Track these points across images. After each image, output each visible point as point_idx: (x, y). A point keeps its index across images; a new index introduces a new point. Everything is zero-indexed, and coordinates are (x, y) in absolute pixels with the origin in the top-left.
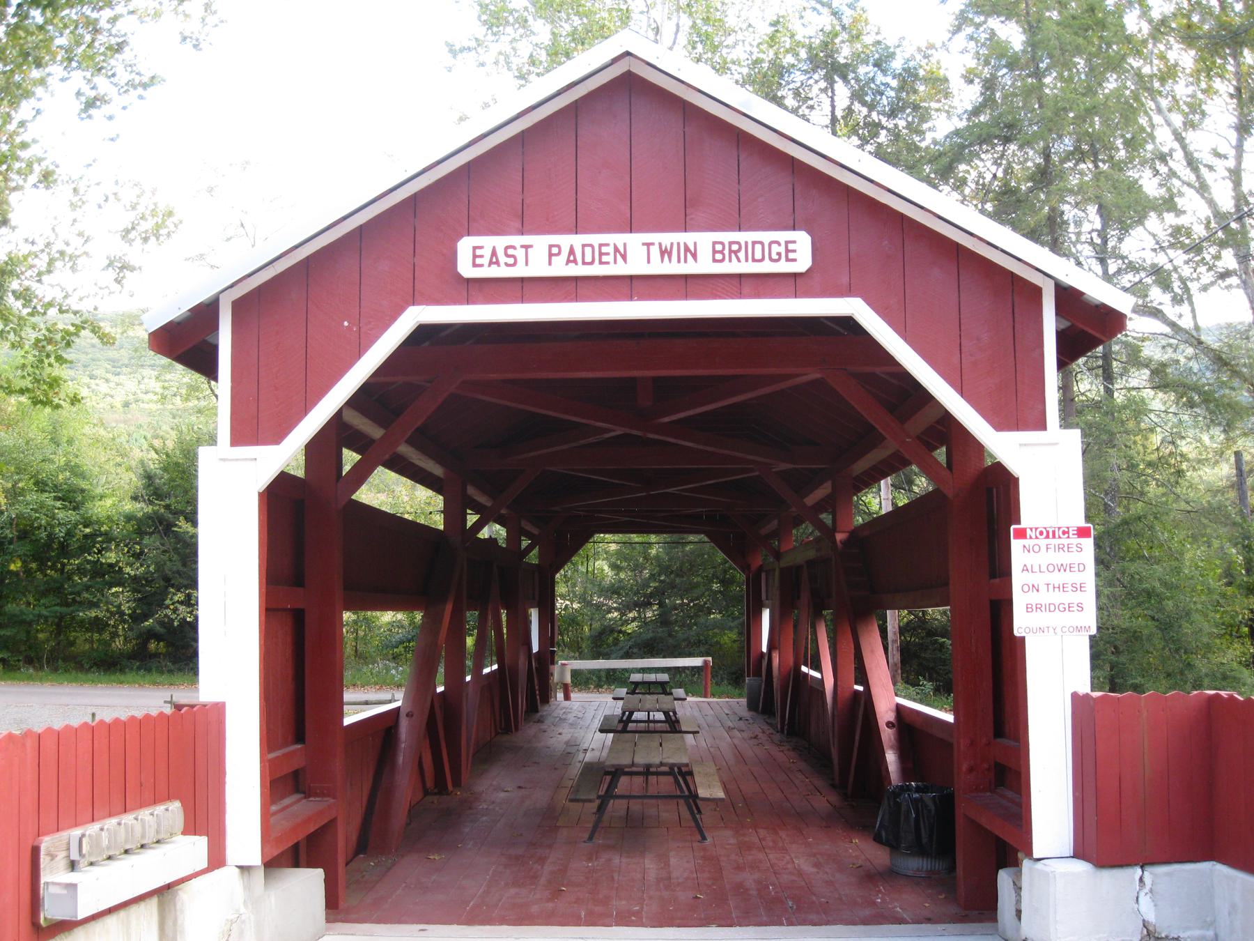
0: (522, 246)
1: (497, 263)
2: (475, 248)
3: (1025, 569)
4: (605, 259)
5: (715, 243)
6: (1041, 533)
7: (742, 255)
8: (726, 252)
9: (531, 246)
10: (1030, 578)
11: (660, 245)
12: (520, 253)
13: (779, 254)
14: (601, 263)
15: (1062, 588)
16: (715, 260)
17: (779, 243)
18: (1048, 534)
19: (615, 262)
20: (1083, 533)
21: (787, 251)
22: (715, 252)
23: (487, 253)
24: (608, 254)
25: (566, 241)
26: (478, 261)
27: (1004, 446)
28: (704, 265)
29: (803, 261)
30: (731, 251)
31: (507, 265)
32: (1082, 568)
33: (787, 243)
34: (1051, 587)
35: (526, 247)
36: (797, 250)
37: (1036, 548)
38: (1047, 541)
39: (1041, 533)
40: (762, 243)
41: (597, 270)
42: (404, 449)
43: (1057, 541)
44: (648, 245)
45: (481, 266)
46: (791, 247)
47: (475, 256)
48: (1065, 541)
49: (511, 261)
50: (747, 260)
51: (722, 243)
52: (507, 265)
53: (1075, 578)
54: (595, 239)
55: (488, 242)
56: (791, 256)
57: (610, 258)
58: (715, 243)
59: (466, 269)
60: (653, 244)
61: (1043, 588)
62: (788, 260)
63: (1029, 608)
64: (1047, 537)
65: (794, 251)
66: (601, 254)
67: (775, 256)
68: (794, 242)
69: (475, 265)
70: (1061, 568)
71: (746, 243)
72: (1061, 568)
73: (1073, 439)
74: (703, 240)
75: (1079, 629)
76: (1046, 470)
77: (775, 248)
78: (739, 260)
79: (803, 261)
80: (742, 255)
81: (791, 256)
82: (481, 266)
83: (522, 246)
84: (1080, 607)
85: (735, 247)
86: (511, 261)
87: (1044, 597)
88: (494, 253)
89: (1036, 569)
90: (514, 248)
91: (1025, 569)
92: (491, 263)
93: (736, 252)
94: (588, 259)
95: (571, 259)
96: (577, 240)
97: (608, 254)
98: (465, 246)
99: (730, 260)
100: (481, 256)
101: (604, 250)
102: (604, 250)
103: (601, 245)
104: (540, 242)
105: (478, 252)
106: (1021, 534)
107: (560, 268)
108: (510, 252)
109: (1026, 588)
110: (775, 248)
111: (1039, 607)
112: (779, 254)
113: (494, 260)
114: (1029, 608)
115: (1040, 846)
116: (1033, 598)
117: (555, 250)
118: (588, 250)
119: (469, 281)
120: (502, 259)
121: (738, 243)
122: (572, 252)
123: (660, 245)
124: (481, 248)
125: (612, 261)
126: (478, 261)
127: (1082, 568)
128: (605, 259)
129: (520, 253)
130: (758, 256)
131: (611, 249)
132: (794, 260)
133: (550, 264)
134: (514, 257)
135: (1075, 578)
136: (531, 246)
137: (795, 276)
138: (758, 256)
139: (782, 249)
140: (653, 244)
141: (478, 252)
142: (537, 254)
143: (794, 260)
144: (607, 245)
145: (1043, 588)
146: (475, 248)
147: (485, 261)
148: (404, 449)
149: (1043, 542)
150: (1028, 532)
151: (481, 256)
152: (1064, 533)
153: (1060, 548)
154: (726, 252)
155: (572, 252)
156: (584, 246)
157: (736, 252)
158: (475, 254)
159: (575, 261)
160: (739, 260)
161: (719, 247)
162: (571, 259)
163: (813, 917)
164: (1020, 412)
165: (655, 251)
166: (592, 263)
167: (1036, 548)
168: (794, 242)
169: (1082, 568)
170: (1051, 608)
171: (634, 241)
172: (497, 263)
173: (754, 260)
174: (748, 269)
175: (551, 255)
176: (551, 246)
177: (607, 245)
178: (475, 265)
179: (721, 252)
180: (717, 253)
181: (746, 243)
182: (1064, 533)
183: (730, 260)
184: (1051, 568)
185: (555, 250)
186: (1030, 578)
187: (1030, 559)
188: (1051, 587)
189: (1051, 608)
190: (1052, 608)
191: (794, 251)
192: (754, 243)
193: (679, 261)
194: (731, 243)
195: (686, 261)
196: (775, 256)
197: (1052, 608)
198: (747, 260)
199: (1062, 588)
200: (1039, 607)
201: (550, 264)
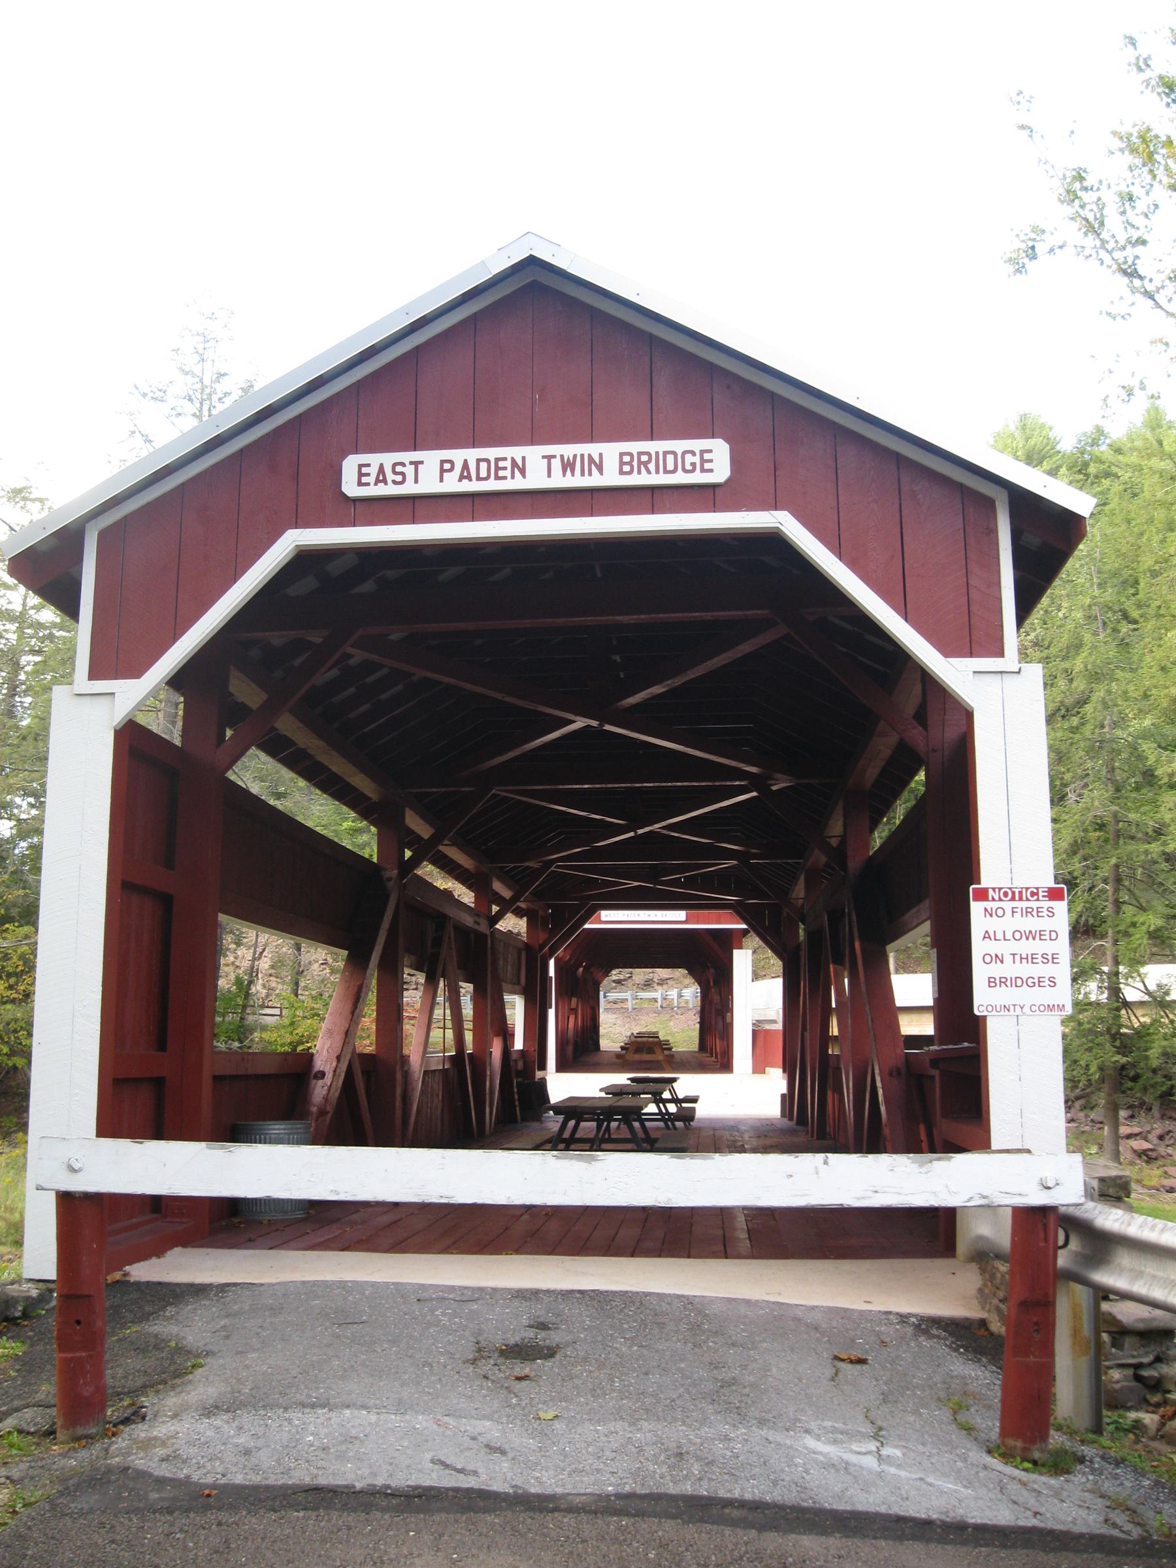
0: (411, 463)
1: (385, 481)
2: (360, 466)
3: (986, 936)
4: (501, 473)
5: (622, 455)
6: (1006, 894)
7: (652, 466)
8: (635, 463)
9: (422, 463)
10: (992, 947)
11: (562, 457)
12: (409, 471)
13: (693, 464)
14: (497, 478)
15: (1031, 958)
16: (622, 472)
17: (693, 453)
18: (1014, 895)
19: (513, 477)
20: (1054, 895)
21: (703, 461)
22: (622, 463)
23: (373, 470)
24: (505, 468)
25: (458, 455)
26: (364, 480)
27: (955, 673)
28: (611, 478)
29: (720, 470)
30: (640, 463)
31: (394, 482)
32: (1053, 935)
33: (702, 452)
34: (1017, 958)
35: (416, 464)
36: (715, 459)
37: (1000, 912)
38: (1014, 904)
39: (1006, 894)
40: (674, 453)
41: (492, 485)
42: (287, 725)
43: (1024, 904)
44: (549, 458)
45: (368, 484)
46: (707, 456)
47: (361, 475)
48: (1035, 905)
49: (399, 478)
50: (657, 472)
51: (631, 454)
52: (394, 482)
53: (1047, 947)
54: (491, 453)
55: (375, 460)
56: (707, 466)
57: (508, 473)
58: (622, 455)
59: (350, 488)
60: (554, 457)
61: (1008, 959)
62: (703, 470)
63: (991, 982)
64: (1013, 899)
65: (711, 461)
66: (497, 469)
67: (688, 467)
68: (710, 451)
69: (360, 484)
70: (1030, 936)
71: (657, 453)
72: (1030, 936)
73: (1035, 672)
74: (610, 451)
75: (1050, 1008)
76: (1005, 707)
77: (689, 459)
78: (649, 472)
79: (720, 470)
80: (652, 466)
81: (707, 466)
82: (368, 484)
83: (411, 463)
84: (1053, 982)
85: (644, 458)
86: (399, 478)
87: (1008, 969)
88: (381, 469)
89: (1000, 936)
90: (403, 464)
91: (986, 936)
92: (377, 482)
93: (646, 464)
94: (483, 474)
95: (465, 475)
96: (471, 455)
97: (505, 468)
98: (350, 465)
99: (639, 472)
100: (368, 475)
101: (501, 464)
102: (501, 464)
103: (497, 460)
104: (431, 458)
105: (364, 470)
106: (982, 895)
107: (452, 484)
108: (399, 469)
109: (988, 959)
110: (689, 459)
111: (1003, 981)
112: (693, 464)
113: (381, 478)
114: (991, 982)
115: (993, 867)
116: (997, 970)
117: (447, 466)
118: (484, 465)
119: (356, 501)
120: (390, 476)
121: (649, 454)
122: (466, 465)
123: (562, 457)
124: (368, 465)
125: (509, 476)
126: (364, 480)
127: (1053, 935)
128: (501, 473)
129: (409, 471)
130: (670, 467)
131: (508, 464)
132: (711, 471)
133: (441, 480)
134: (403, 474)
135: (1047, 947)
136: (422, 463)
137: (713, 487)
138: (670, 467)
139: (697, 459)
140: (554, 457)
141: (364, 470)
142: (429, 471)
143: (711, 471)
144: (505, 459)
145: (1008, 959)
146: (360, 466)
147: (371, 480)
148: (287, 725)
149: (1008, 905)
150: (991, 891)
151: (368, 475)
152: (1033, 894)
153: (1028, 912)
154: (635, 463)
155: (466, 465)
156: (479, 461)
157: (646, 464)
158: (359, 473)
159: (469, 478)
160: (649, 472)
161: (626, 459)
162: (465, 475)
163: (742, 1310)
164: (975, 637)
165: (556, 464)
166: (487, 478)
167: (1000, 912)
168: (710, 451)
169: (1054, 935)
170: (1016, 982)
171: (533, 454)
172: (385, 481)
173: (666, 471)
174: (655, 479)
175: (442, 471)
176: (443, 462)
177: (505, 459)
178: (360, 484)
179: (630, 463)
180: (625, 464)
181: (657, 453)
182: (1033, 894)
183: (639, 472)
184: (1017, 935)
185: (447, 466)
186: (992, 947)
187: (993, 924)
188: (1017, 958)
189: (1016, 982)
190: (1019, 982)
191: (711, 461)
192: (665, 453)
193: (583, 474)
194: (640, 454)
195: (590, 474)
196: (688, 467)
197: (1019, 982)
198: (657, 472)
199: (1031, 958)
200: (1003, 981)
201: (441, 480)
